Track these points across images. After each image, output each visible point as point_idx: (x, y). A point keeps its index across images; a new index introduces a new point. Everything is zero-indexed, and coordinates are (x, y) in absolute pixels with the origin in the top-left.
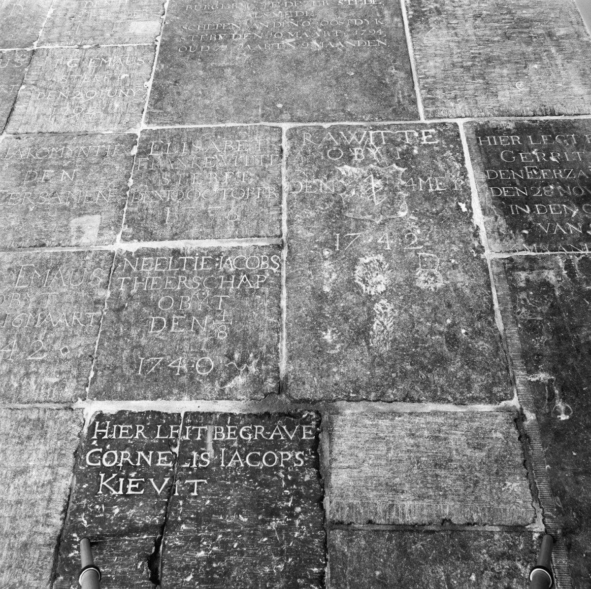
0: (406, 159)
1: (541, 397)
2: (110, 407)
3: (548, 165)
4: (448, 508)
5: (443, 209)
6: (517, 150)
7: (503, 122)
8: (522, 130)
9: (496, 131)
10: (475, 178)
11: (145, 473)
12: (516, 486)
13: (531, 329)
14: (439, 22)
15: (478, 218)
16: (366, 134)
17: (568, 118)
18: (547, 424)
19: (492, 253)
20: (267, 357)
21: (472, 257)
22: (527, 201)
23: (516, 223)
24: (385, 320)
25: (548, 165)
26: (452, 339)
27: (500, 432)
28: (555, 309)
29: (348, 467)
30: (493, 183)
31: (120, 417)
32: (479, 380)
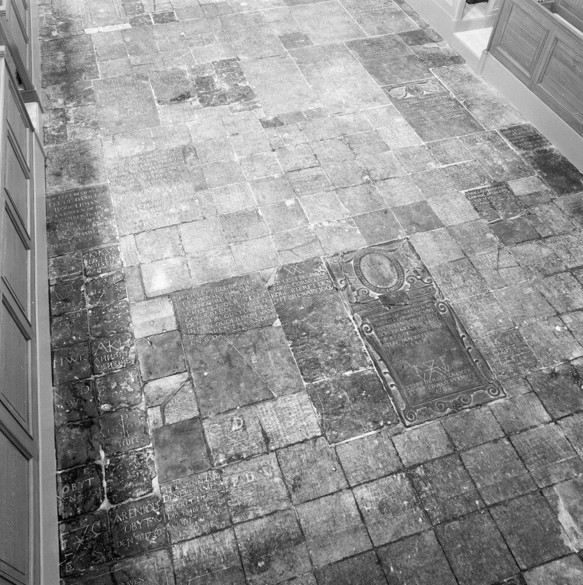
0: (489, 139)
1: (540, 173)
2: (467, 191)
3: (519, 135)
4: (534, 190)
5: (503, 147)
6: (511, 133)
7: (504, 128)
8: (510, 129)
9: (504, 130)
10: (506, 140)
11: (481, 198)
12: (543, 186)
13: (533, 164)
15: (511, 148)
16: (477, 135)
17: (7, 169)
18: (543, 177)
19: (518, 153)
20: (488, 177)
21: (515, 155)
22: (519, 143)
23: (519, 147)
24: (505, 167)
25: (519, 135)
26: (520, 169)
27: (536, 179)
28: (535, 160)
29: (299, 170)
30: (510, 141)
31: (469, 192)
32: (528, 173)
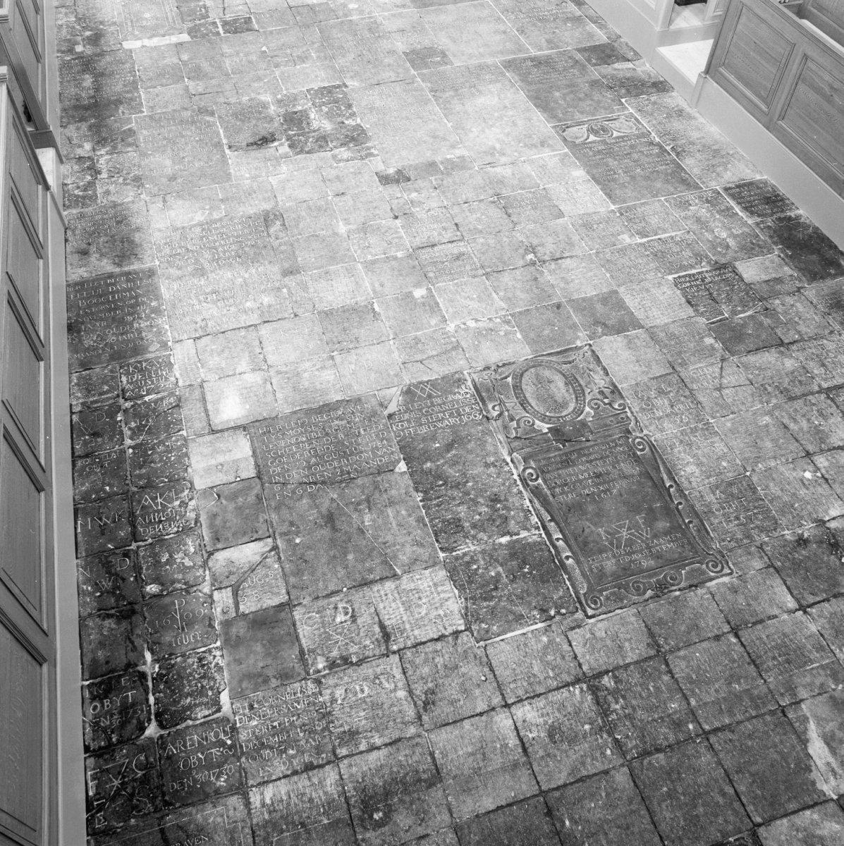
0: (708, 201)
1: (782, 251)
2: (676, 276)
3: (751, 196)
4: (774, 275)
5: (728, 212)
6: (740, 193)
7: (730, 185)
8: (738, 186)
9: (730, 188)
10: (732, 203)
11: (697, 286)
12: (786, 268)
13: (771, 237)
14: (709, 765)
15: (740, 214)
16: (690, 195)
17: (10, 245)
18: (787, 255)
19: (750, 222)
20: (707, 257)
21: (745, 224)
22: (752, 206)
23: (752, 213)
24: (731, 242)
25: (751, 196)
26: (753, 244)
27: (777, 260)
28: (775, 232)
30: (739, 203)
31: (679, 277)
32: (765, 251)
